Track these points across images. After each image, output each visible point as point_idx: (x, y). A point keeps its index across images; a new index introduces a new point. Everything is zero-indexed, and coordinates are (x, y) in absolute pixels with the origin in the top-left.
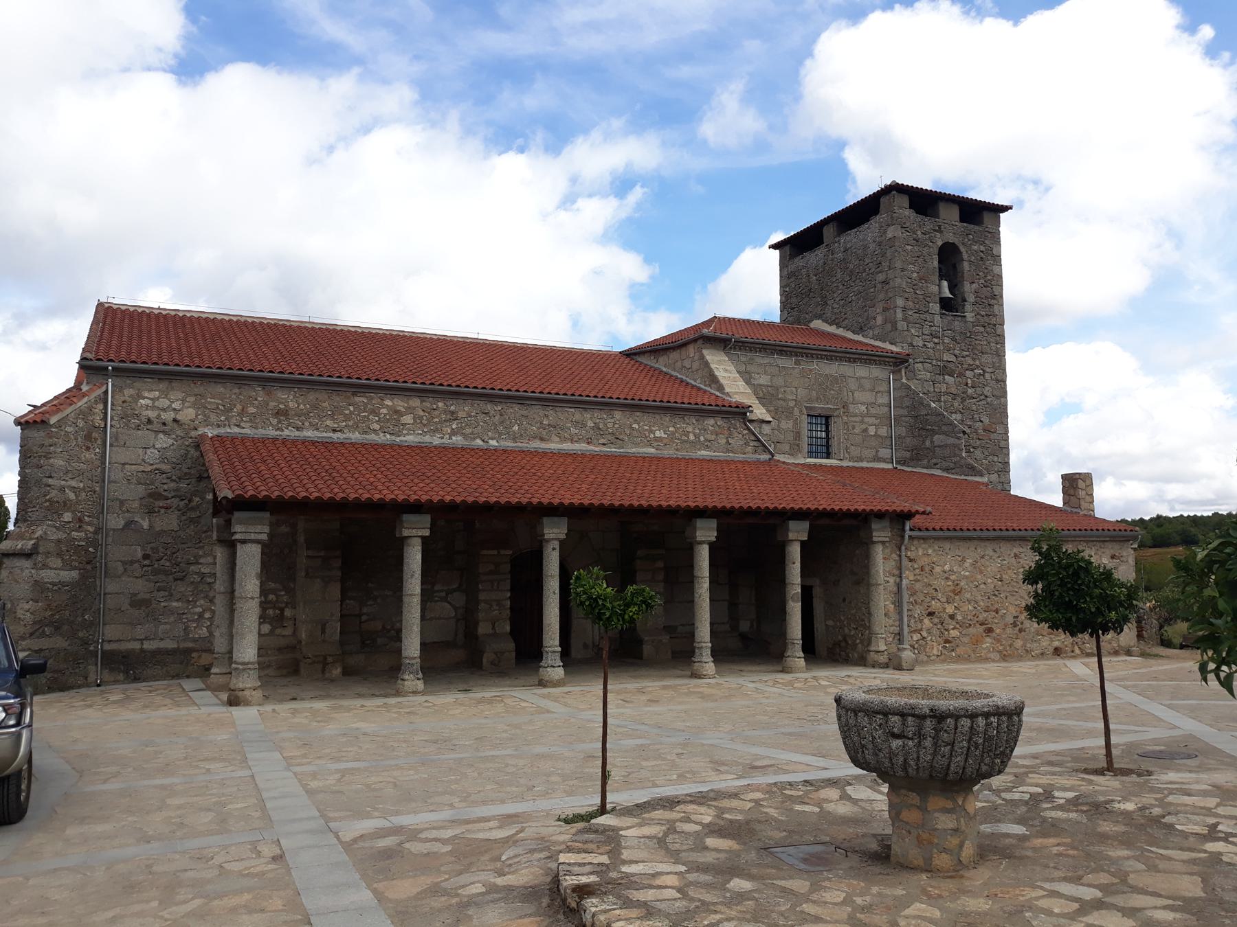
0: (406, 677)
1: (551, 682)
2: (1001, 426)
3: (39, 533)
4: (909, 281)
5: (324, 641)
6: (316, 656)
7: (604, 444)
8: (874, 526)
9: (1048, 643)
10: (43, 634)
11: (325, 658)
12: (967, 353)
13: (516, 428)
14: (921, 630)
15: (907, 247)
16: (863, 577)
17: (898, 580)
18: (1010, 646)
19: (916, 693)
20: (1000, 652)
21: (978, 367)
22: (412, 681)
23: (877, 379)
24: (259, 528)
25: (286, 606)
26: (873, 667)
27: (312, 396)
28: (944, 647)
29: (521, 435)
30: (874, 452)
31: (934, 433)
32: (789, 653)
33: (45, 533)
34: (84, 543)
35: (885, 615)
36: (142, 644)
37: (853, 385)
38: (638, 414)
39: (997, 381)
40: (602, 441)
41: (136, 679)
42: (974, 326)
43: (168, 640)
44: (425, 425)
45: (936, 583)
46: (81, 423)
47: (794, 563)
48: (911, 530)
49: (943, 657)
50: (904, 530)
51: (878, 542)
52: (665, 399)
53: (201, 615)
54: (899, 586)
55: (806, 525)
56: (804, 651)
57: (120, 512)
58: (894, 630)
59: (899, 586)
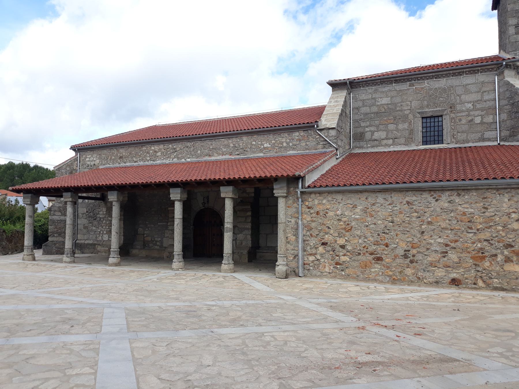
7: (238, 154)
9: (444, 274)
13: (199, 152)
14: (316, 254)
18: (401, 272)
20: (390, 276)
23: (483, 83)
27: (130, 149)
29: (201, 155)
37: (460, 91)
38: (255, 136)
40: (237, 153)
44: (165, 156)
46: (68, 169)
49: (333, 274)
52: (225, 131)
53: (100, 232)
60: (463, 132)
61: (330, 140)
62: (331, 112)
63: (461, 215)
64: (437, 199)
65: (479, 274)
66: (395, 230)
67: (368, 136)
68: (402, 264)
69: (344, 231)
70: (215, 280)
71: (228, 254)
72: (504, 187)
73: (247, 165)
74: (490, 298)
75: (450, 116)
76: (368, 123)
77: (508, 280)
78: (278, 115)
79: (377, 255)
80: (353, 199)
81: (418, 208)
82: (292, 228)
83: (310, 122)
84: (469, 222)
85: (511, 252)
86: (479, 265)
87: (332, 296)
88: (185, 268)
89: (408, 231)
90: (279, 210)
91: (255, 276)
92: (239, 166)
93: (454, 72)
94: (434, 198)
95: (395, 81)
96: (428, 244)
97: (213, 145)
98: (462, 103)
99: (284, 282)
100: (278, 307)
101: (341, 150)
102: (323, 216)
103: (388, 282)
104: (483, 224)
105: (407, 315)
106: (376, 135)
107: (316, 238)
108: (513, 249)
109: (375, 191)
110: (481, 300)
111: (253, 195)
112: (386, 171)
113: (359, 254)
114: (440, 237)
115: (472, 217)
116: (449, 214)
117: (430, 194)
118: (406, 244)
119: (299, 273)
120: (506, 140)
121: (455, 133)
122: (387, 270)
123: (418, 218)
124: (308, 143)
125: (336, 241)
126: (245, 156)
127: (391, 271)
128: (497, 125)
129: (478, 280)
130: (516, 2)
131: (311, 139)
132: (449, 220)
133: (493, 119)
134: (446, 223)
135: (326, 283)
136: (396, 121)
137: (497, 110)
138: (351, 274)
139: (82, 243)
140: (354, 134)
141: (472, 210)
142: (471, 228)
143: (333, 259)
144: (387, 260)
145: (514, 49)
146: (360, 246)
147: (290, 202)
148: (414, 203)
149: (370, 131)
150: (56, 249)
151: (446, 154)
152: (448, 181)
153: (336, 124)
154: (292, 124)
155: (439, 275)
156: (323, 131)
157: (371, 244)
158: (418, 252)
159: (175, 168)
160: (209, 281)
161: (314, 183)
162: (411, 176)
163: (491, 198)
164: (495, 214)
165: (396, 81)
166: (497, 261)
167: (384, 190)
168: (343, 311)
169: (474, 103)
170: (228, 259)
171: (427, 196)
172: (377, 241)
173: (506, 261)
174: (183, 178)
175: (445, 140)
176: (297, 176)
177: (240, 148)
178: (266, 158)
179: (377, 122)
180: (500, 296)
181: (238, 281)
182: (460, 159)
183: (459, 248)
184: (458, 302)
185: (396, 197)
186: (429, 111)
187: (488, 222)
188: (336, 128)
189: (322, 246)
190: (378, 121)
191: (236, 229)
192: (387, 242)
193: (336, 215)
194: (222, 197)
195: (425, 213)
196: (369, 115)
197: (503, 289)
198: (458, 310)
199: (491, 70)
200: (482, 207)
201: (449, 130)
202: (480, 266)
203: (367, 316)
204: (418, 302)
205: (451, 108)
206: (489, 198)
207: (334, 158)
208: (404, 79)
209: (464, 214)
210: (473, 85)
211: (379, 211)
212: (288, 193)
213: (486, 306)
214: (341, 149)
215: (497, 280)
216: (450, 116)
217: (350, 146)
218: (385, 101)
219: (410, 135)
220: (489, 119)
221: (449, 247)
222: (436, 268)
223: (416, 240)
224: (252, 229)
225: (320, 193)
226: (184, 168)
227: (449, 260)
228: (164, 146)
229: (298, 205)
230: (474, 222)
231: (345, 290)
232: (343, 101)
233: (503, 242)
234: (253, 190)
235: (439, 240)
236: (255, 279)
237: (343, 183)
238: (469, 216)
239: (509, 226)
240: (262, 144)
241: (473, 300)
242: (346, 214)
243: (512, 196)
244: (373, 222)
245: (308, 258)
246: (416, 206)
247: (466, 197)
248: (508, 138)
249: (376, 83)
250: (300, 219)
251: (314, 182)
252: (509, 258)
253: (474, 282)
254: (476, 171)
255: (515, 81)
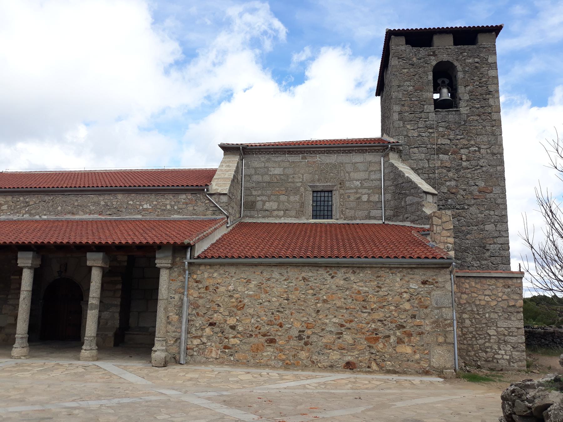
2: (498, 188)
4: (406, 92)
7: (110, 215)
9: (339, 357)
12: (462, 136)
13: (59, 208)
14: (202, 336)
15: (404, 70)
18: (294, 356)
21: (472, 145)
23: (370, 162)
30: (366, 212)
31: (406, 195)
37: (349, 168)
38: (133, 195)
39: (493, 154)
40: (109, 213)
42: (468, 116)
44: (12, 210)
45: (218, 300)
56: (97, 345)
60: (351, 209)
61: (221, 207)
62: (222, 176)
63: (356, 293)
64: (333, 276)
65: (373, 356)
66: (290, 309)
67: (259, 205)
68: (296, 346)
69: (235, 310)
70: (73, 371)
71: (91, 337)
72: (396, 266)
73: (122, 228)
74: (385, 382)
75: (339, 192)
76: (260, 192)
77: (400, 362)
78: (160, 173)
79: (269, 337)
80: (247, 273)
81: (314, 284)
82: (175, 306)
83: (199, 185)
84: (363, 301)
85: (403, 333)
86: (373, 347)
87: (222, 387)
88: (30, 356)
89: (303, 310)
90: (160, 283)
91: (125, 364)
92: (111, 228)
93: (345, 149)
94: (330, 275)
95: (288, 152)
96: (323, 324)
97: (79, 201)
98: (351, 180)
99: (162, 372)
100: (162, 405)
101: (231, 218)
102: (213, 292)
103: (281, 368)
104: (377, 304)
105: (311, 408)
106: (268, 205)
107: (203, 317)
108: (405, 330)
109: (271, 264)
110: (378, 385)
111: (126, 264)
112: (281, 244)
113: (251, 335)
114: (335, 317)
115: (367, 296)
116: (344, 292)
117: (327, 271)
118: (301, 324)
119: (180, 360)
120: (390, 219)
121: (344, 209)
122: (280, 354)
123: (313, 295)
124: (195, 208)
125: (226, 321)
126: (119, 218)
127: (284, 354)
128: (382, 204)
129: (372, 363)
130: (400, 91)
131: (199, 203)
132: (345, 299)
133: (379, 198)
134: (341, 302)
135: (213, 371)
136: (287, 192)
137: (383, 190)
138: (241, 360)
140: (245, 202)
141: (367, 289)
142: (365, 308)
143: (221, 342)
144: (281, 342)
145: (397, 134)
146: (252, 327)
147: (175, 274)
148: (309, 279)
149: (261, 200)
151: (336, 229)
152: (329, 257)
153: (228, 190)
154: (160, 185)
155: (334, 358)
156: (214, 196)
157: (263, 325)
158: (313, 333)
159: (25, 226)
160: (64, 373)
161: (204, 253)
162: (294, 250)
163: (385, 278)
164: (388, 294)
165: (290, 153)
166: (390, 343)
167: (280, 265)
168: (239, 407)
169: (362, 181)
170: (91, 344)
171: (323, 273)
172: (270, 321)
173: (398, 343)
174: (38, 239)
175: (334, 215)
176: (186, 244)
177: (112, 207)
178: (145, 221)
179: (269, 192)
180: (394, 380)
181: (103, 372)
182: (350, 236)
183: (354, 329)
184: (356, 389)
185: (292, 273)
186: (320, 185)
187: (382, 302)
188: (228, 194)
189: (209, 327)
190: (270, 191)
191: (103, 306)
192: (281, 321)
193: (228, 290)
194: (88, 265)
195: (320, 290)
196: (261, 184)
197: (395, 372)
198: (360, 398)
199: (377, 151)
200: (377, 285)
201: (338, 206)
202: (374, 348)
203: (268, 412)
204: (317, 391)
205: (340, 184)
206: (382, 276)
207: (225, 227)
208: (297, 151)
209: (359, 292)
210: (361, 164)
211: (274, 287)
212: (173, 263)
213: (384, 392)
214: (231, 216)
215: (390, 363)
216: (339, 192)
217: (241, 215)
218: (278, 171)
219: (301, 208)
220: (375, 198)
221: (344, 328)
222: (331, 350)
223: (311, 320)
224: (122, 305)
225: (211, 265)
226: (39, 227)
227: (344, 341)
228: (13, 197)
229: (185, 278)
230: (368, 301)
231: (235, 379)
232: (235, 166)
233: (395, 323)
234: (125, 258)
235: (335, 320)
236: (125, 368)
237: (237, 255)
238: (363, 295)
239: (401, 306)
240: (141, 205)
241: (370, 386)
242: (239, 290)
243: (404, 276)
244: (268, 300)
245: (192, 342)
246: (312, 282)
247: (361, 275)
248: (392, 217)
249: (269, 151)
250: (185, 295)
251: (204, 252)
252: (401, 339)
253: (368, 365)
254: (368, 248)
255: (398, 164)
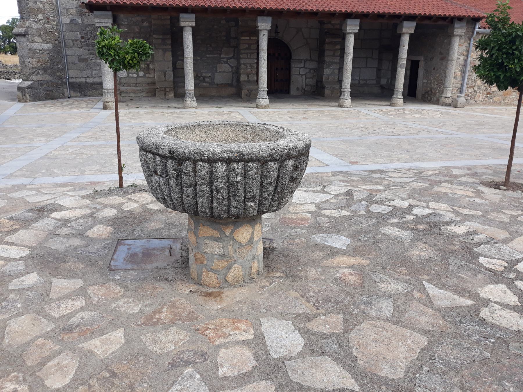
0: (187, 99)
1: (261, 106)
3: (27, 24)
5: (165, 81)
6: (161, 88)
8: (456, 26)
10: (38, 73)
11: (165, 89)
14: (474, 86)
16: (445, 57)
17: (466, 58)
19: (246, 130)
22: (191, 102)
24: (106, 20)
25: (150, 63)
26: (442, 105)
28: (487, 97)
32: (394, 96)
33: (30, 24)
34: (52, 30)
35: (454, 77)
36: (86, 79)
41: (85, 96)
43: (98, 78)
47: (404, 46)
48: (479, 28)
50: (474, 28)
51: (457, 35)
54: (466, 61)
55: (413, 24)
56: (403, 95)
57: (67, 15)
58: (458, 86)
59: (466, 61)
139: (82, 83)
150: (45, 93)
